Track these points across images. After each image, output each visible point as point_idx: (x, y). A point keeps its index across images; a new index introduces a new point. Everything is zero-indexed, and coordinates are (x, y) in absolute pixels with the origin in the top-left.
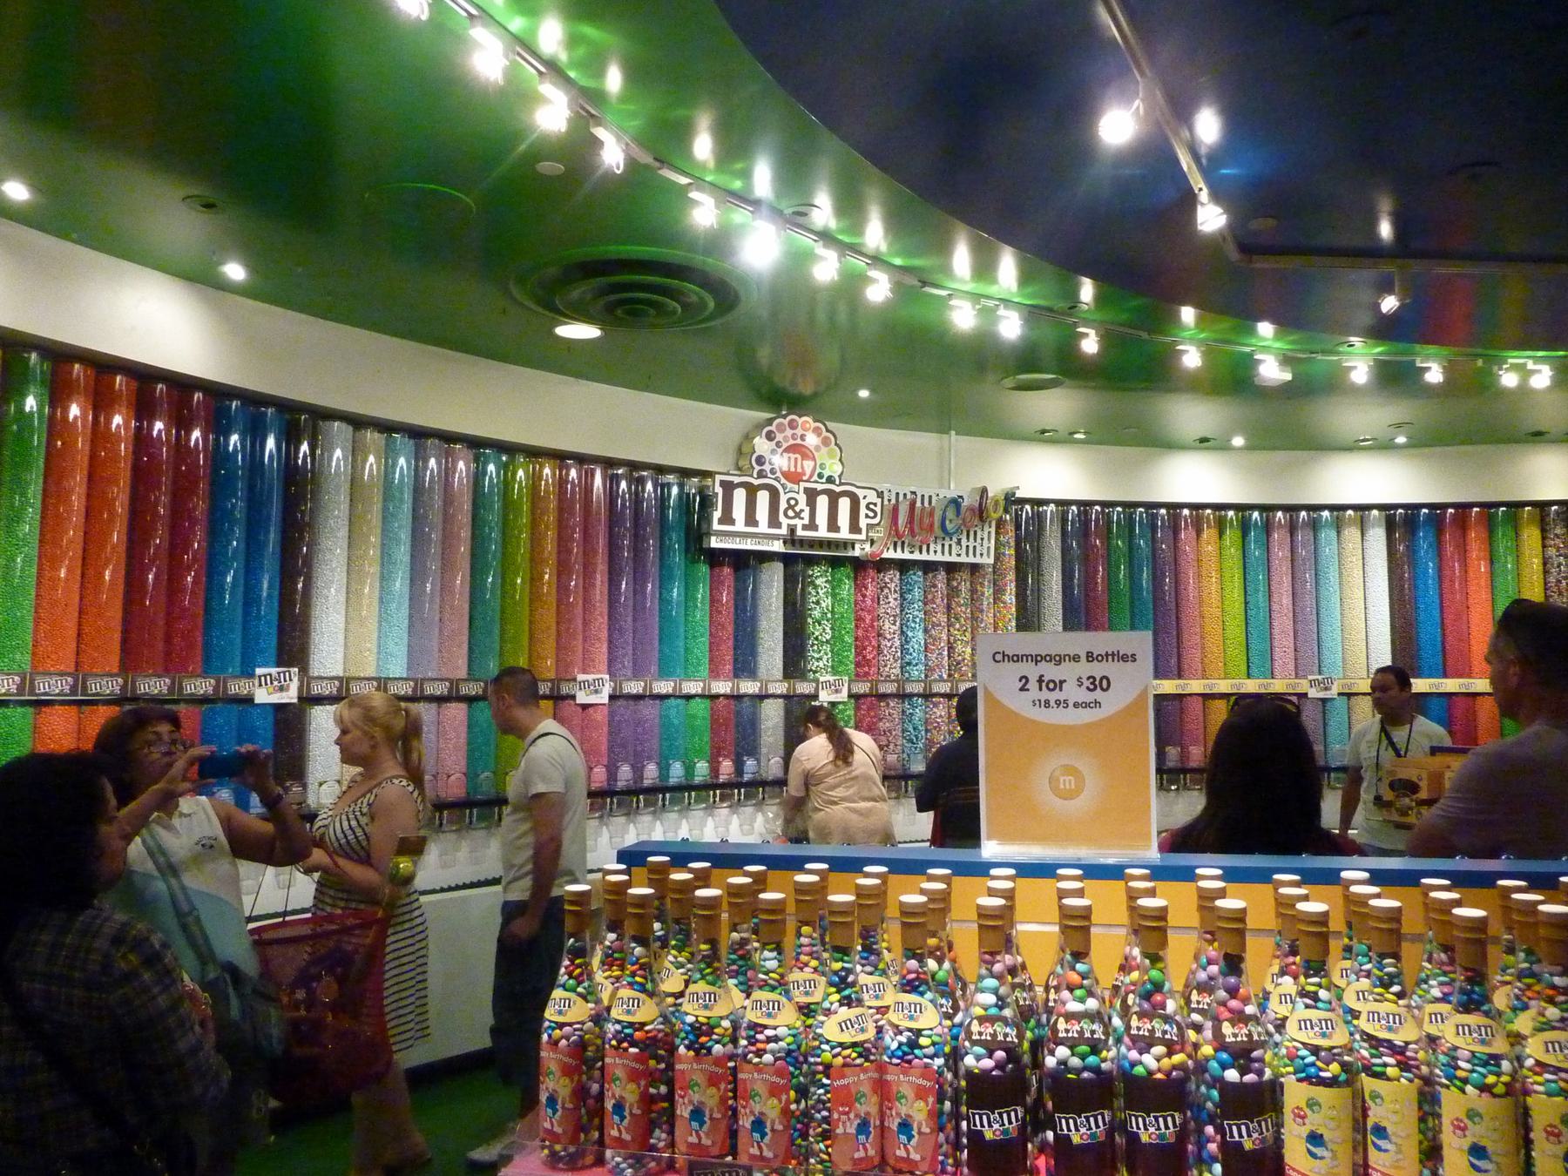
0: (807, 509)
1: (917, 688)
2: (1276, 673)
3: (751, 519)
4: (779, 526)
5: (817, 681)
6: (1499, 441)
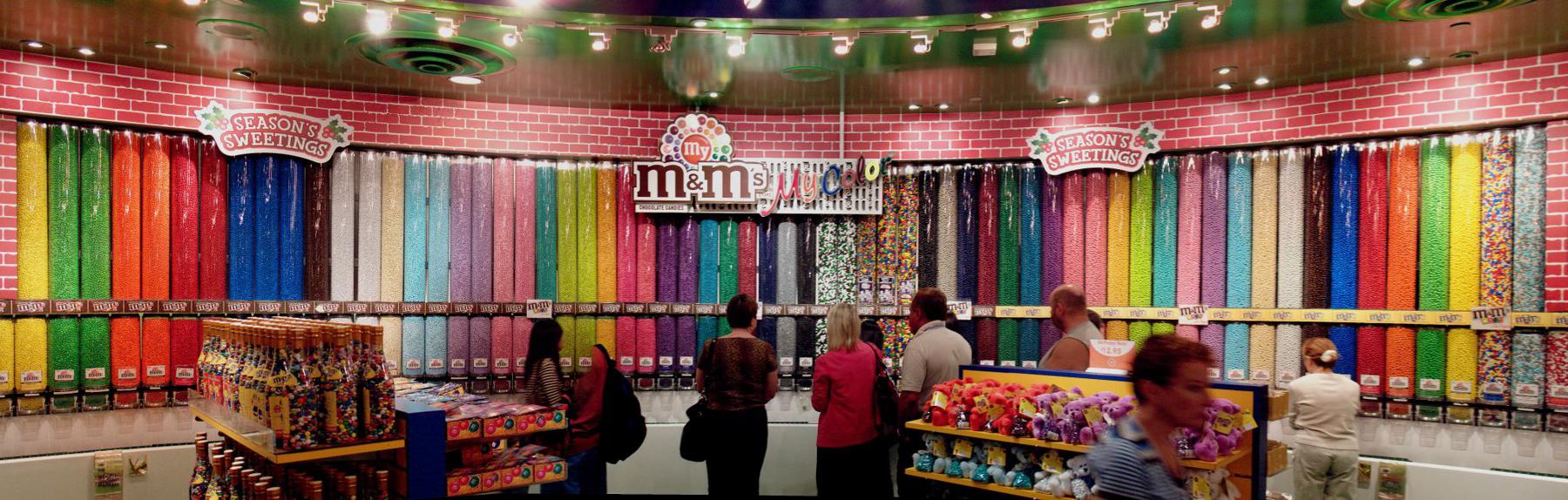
0: (706, 183)
2: (1110, 298)
3: (662, 191)
6: (1185, 97)
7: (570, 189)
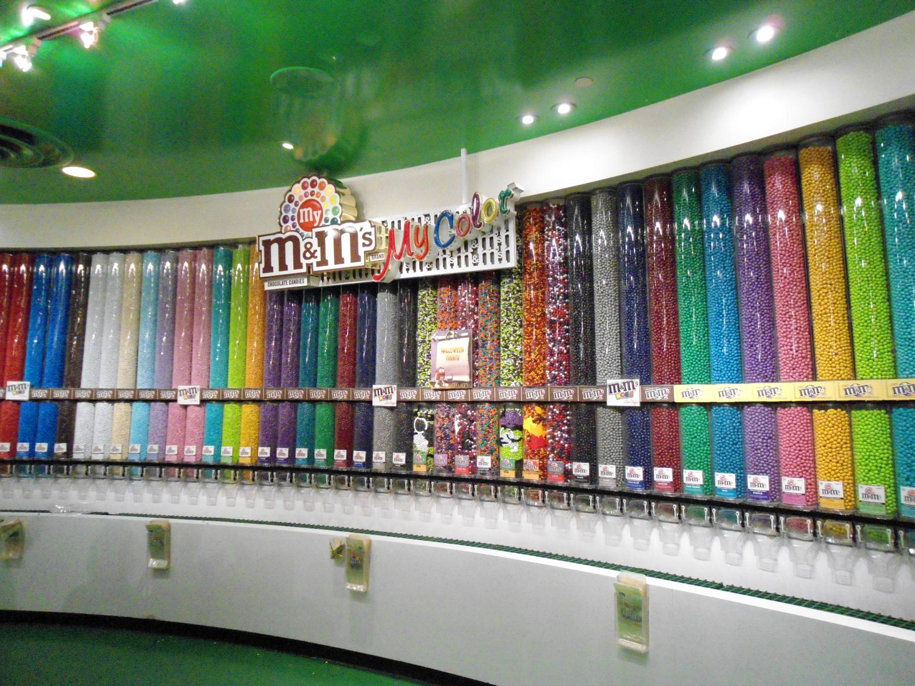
0: (319, 249)
1: (233, 395)
2: (820, 371)
3: (283, 266)
4: (300, 266)
5: (176, 390)
7: (321, 371)
